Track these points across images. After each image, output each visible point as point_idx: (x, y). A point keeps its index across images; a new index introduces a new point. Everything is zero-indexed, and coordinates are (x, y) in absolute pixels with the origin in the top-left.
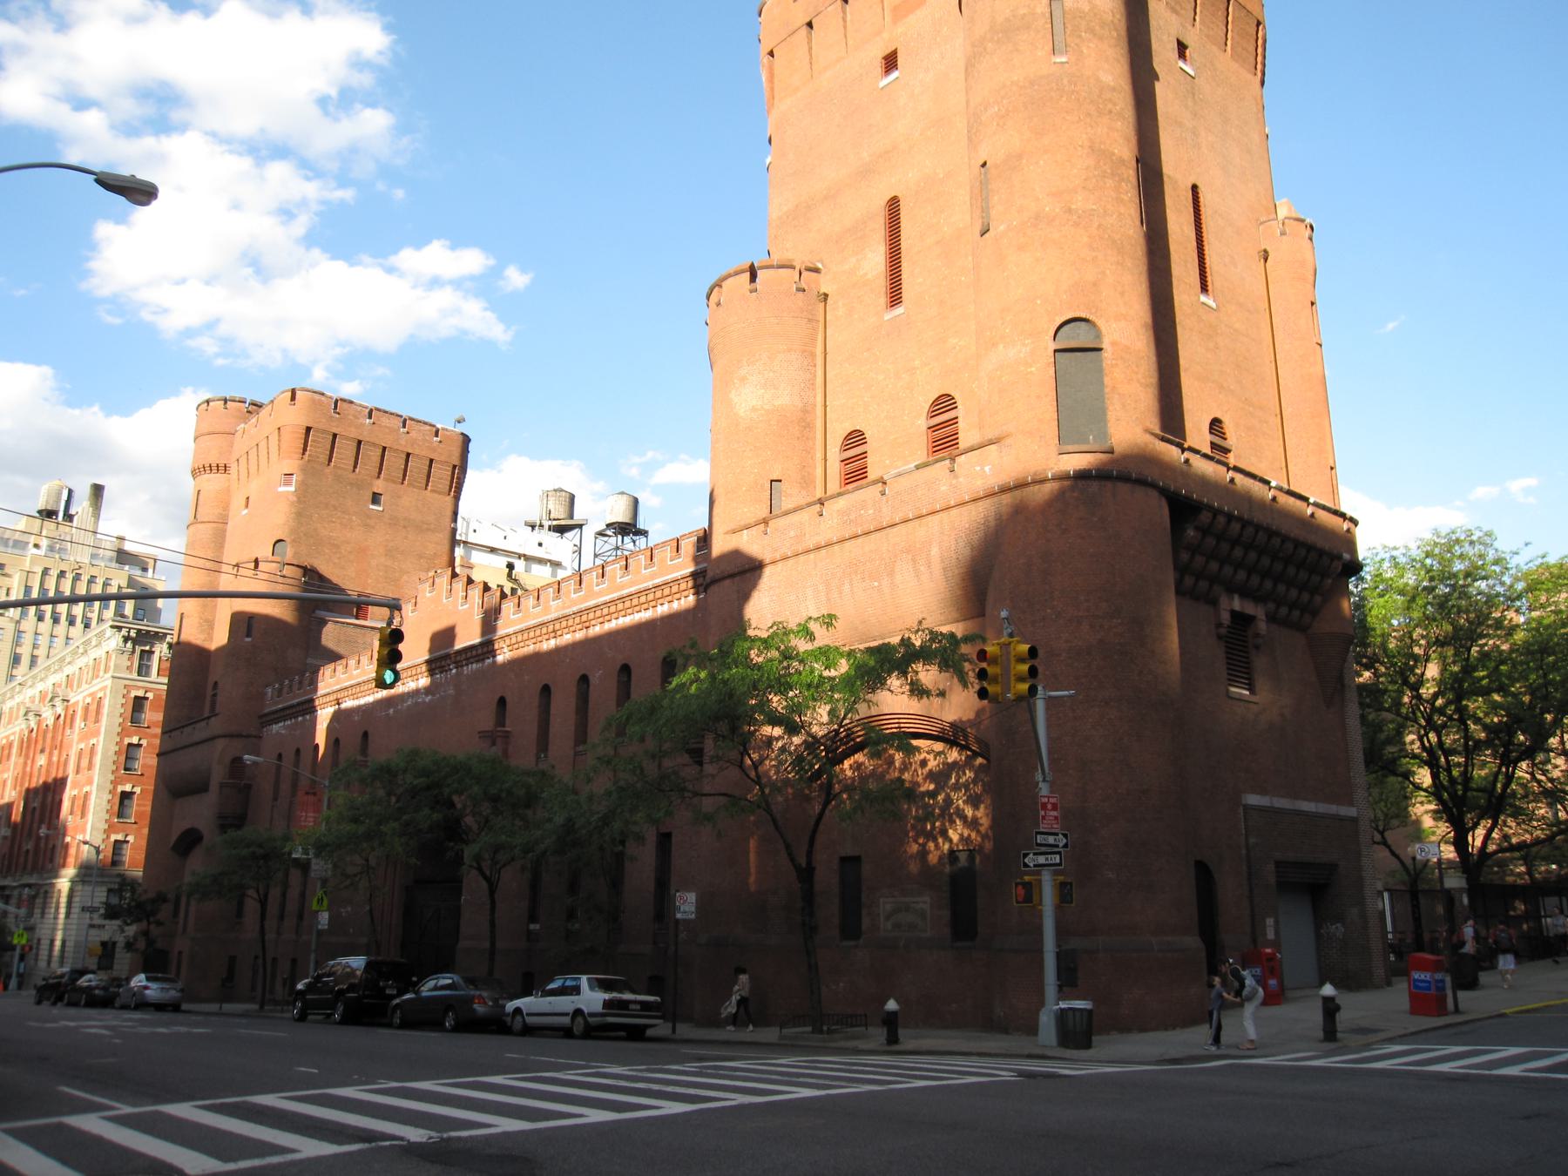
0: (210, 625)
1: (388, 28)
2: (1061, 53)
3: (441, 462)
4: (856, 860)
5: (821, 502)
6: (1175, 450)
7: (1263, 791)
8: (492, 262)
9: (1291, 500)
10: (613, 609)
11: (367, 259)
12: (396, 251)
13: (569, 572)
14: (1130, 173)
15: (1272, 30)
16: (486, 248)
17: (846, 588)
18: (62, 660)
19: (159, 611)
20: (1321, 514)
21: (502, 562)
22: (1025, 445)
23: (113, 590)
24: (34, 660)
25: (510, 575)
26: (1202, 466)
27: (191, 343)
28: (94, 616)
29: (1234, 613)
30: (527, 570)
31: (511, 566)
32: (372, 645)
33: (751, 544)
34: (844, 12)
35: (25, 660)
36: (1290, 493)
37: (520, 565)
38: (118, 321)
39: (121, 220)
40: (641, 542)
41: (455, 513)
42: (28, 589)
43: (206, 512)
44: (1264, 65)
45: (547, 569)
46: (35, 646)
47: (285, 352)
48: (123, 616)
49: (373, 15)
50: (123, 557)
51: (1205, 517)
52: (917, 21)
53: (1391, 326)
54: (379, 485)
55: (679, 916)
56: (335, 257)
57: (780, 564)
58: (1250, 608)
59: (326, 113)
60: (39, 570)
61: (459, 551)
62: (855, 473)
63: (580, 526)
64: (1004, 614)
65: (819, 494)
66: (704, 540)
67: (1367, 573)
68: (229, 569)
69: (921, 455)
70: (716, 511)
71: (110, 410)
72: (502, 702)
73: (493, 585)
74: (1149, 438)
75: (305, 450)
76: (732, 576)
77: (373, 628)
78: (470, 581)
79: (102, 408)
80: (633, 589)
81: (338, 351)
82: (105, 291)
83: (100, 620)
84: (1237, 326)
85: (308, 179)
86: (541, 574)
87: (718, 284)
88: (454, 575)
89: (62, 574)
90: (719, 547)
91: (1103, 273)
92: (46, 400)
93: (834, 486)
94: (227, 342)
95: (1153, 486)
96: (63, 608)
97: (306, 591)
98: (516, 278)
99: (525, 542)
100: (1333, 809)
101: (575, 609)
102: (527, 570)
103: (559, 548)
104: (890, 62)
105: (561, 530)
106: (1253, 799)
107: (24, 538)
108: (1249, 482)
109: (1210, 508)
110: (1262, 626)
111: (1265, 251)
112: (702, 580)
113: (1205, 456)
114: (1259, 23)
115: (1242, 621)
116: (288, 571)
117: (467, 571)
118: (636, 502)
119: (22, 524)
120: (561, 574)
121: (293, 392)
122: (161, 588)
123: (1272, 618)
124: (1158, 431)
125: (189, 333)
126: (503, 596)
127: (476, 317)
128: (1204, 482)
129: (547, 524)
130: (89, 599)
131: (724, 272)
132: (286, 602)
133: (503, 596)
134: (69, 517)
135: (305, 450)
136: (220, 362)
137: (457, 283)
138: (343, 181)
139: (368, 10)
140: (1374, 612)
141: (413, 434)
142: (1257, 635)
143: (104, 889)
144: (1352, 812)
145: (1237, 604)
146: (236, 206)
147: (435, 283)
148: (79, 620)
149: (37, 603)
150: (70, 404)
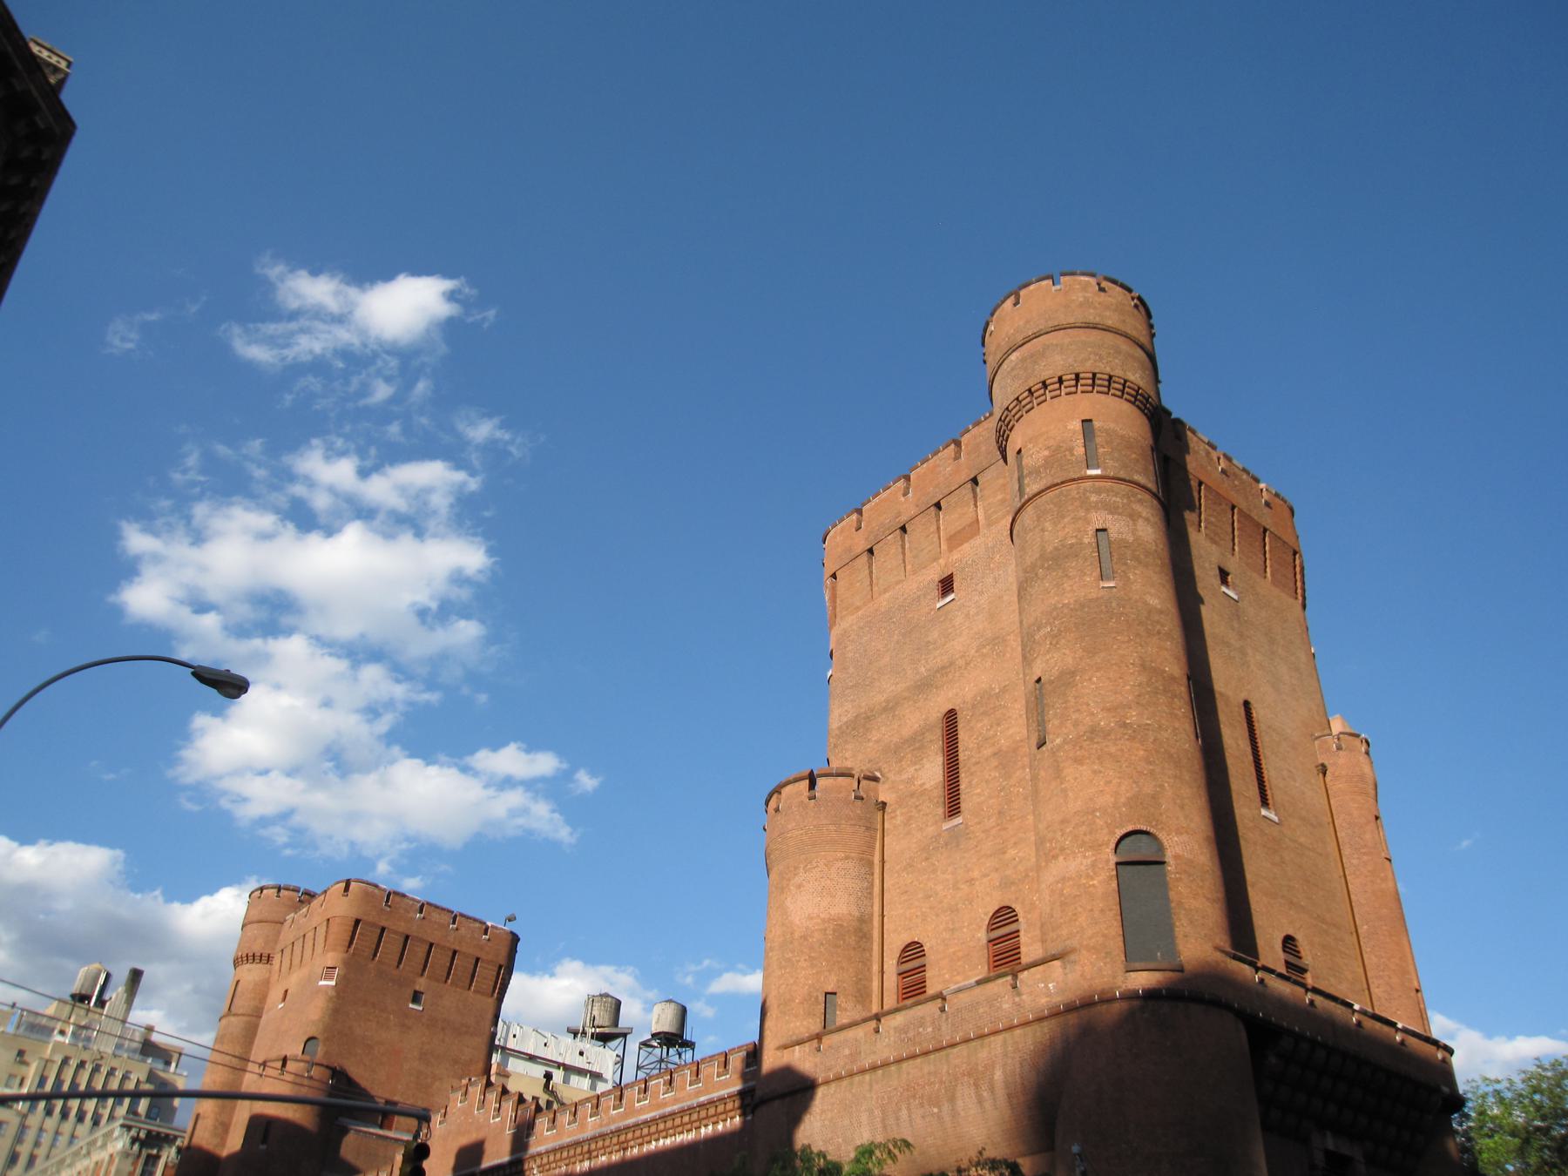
0: (224, 1128)
1: (491, 552)
2: (1109, 579)
3: (489, 962)
5: (877, 1017)
6: (1247, 969)
8: (565, 766)
9: (1378, 1025)
10: (653, 1129)
11: (443, 758)
12: (472, 752)
13: (609, 1086)
14: (1182, 689)
15: (1310, 557)
16: (560, 752)
17: (904, 1113)
18: (62, 1161)
19: (173, 1110)
20: (1412, 1041)
21: (538, 1071)
22: (1086, 959)
23: (130, 1086)
24: (32, 1160)
25: (547, 1086)
26: (1275, 984)
27: (263, 832)
28: (106, 1113)
29: (1329, 1154)
30: (566, 1081)
31: (548, 1076)
32: (392, 1160)
33: (803, 1060)
34: (903, 540)
35: (23, 1161)
36: (1376, 1017)
37: (558, 1075)
38: (196, 808)
39: (218, 712)
40: (688, 1055)
41: (497, 1016)
42: (42, 1081)
43: (242, 1004)
44: (1304, 590)
45: (585, 1083)
46: (37, 1144)
47: (352, 844)
48: (136, 1114)
49: (479, 539)
50: (148, 1048)
52: (969, 550)
53: (1465, 844)
54: (421, 984)
56: (412, 755)
57: (833, 1085)
58: (1346, 1148)
59: (423, 622)
60: (59, 1059)
61: (496, 1058)
62: (913, 988)
63: (625, 1035)
64: (1075, 1149)
65: (875, 1009)
66: (754, 1055)
67: (1471, 1108)
68: (256, 1069)
69: (982, 971)
70: (768, 1024)
71: (170, 898)
73: (528, 1098)
74: (1219, 956)
75: (351, 943)
76: (782, 1096)
77: (397, 1140)
78: (505, 1091)
79: (163, 893)
80: (676, 1107)
81: (404, 846)
82: (190, 779)
83: (111, 1118)
84: (1302, 840)
85: (398, 681)
86: (582, 1084)
87: (777, 791)
88: (489, 1084)
89: (82, 1064)
90: (771, 1060)
91: (1162, 786)
92: (112, 882)
93: (890, 1001)
94: (299, 831)
95: (1228, 1007)
96: (74, 1104)
97: (330, 1095)
98: (586, 781)
99: (566, 1050)
101: (613, 1127)
102: (566, 1081)
103: (603, 1059)
104: (947, 585)
105: (604, 1038)
107: (51, 1024)
108: (1331, 1005)
111: (1323, 765)
112: (749, 1100)
113: (1280, 976)
114: (1295, 553)
116: (315, 1072)
117: (502, 1080)
118: (683, 1011)
119: (51, 1009)
120: (602, 1087)
121: (348, 883)
122: (181, 1084)
124: (1229, 949)
125: (264, 822)
126: (538, 1109)
127: (542, 815)
128: (1282, 1004)
129: (590, 1031)
130: (103, 1096)
131: (784, 780)
132: (308, 1108)
133: (538, 1109)
134: (101, 1003)
135: (351, 943)
136: (288, 852)
137: (530, 785)
138: (431, 685)
139: (475, 535)
140: (1485, 1155)
141: (463, 931)
145: (1330, 1143)
146: (327, 704)
147: (507, 783)
148: (89, 1116)
149: (49, 1097)
150: (136, 888)
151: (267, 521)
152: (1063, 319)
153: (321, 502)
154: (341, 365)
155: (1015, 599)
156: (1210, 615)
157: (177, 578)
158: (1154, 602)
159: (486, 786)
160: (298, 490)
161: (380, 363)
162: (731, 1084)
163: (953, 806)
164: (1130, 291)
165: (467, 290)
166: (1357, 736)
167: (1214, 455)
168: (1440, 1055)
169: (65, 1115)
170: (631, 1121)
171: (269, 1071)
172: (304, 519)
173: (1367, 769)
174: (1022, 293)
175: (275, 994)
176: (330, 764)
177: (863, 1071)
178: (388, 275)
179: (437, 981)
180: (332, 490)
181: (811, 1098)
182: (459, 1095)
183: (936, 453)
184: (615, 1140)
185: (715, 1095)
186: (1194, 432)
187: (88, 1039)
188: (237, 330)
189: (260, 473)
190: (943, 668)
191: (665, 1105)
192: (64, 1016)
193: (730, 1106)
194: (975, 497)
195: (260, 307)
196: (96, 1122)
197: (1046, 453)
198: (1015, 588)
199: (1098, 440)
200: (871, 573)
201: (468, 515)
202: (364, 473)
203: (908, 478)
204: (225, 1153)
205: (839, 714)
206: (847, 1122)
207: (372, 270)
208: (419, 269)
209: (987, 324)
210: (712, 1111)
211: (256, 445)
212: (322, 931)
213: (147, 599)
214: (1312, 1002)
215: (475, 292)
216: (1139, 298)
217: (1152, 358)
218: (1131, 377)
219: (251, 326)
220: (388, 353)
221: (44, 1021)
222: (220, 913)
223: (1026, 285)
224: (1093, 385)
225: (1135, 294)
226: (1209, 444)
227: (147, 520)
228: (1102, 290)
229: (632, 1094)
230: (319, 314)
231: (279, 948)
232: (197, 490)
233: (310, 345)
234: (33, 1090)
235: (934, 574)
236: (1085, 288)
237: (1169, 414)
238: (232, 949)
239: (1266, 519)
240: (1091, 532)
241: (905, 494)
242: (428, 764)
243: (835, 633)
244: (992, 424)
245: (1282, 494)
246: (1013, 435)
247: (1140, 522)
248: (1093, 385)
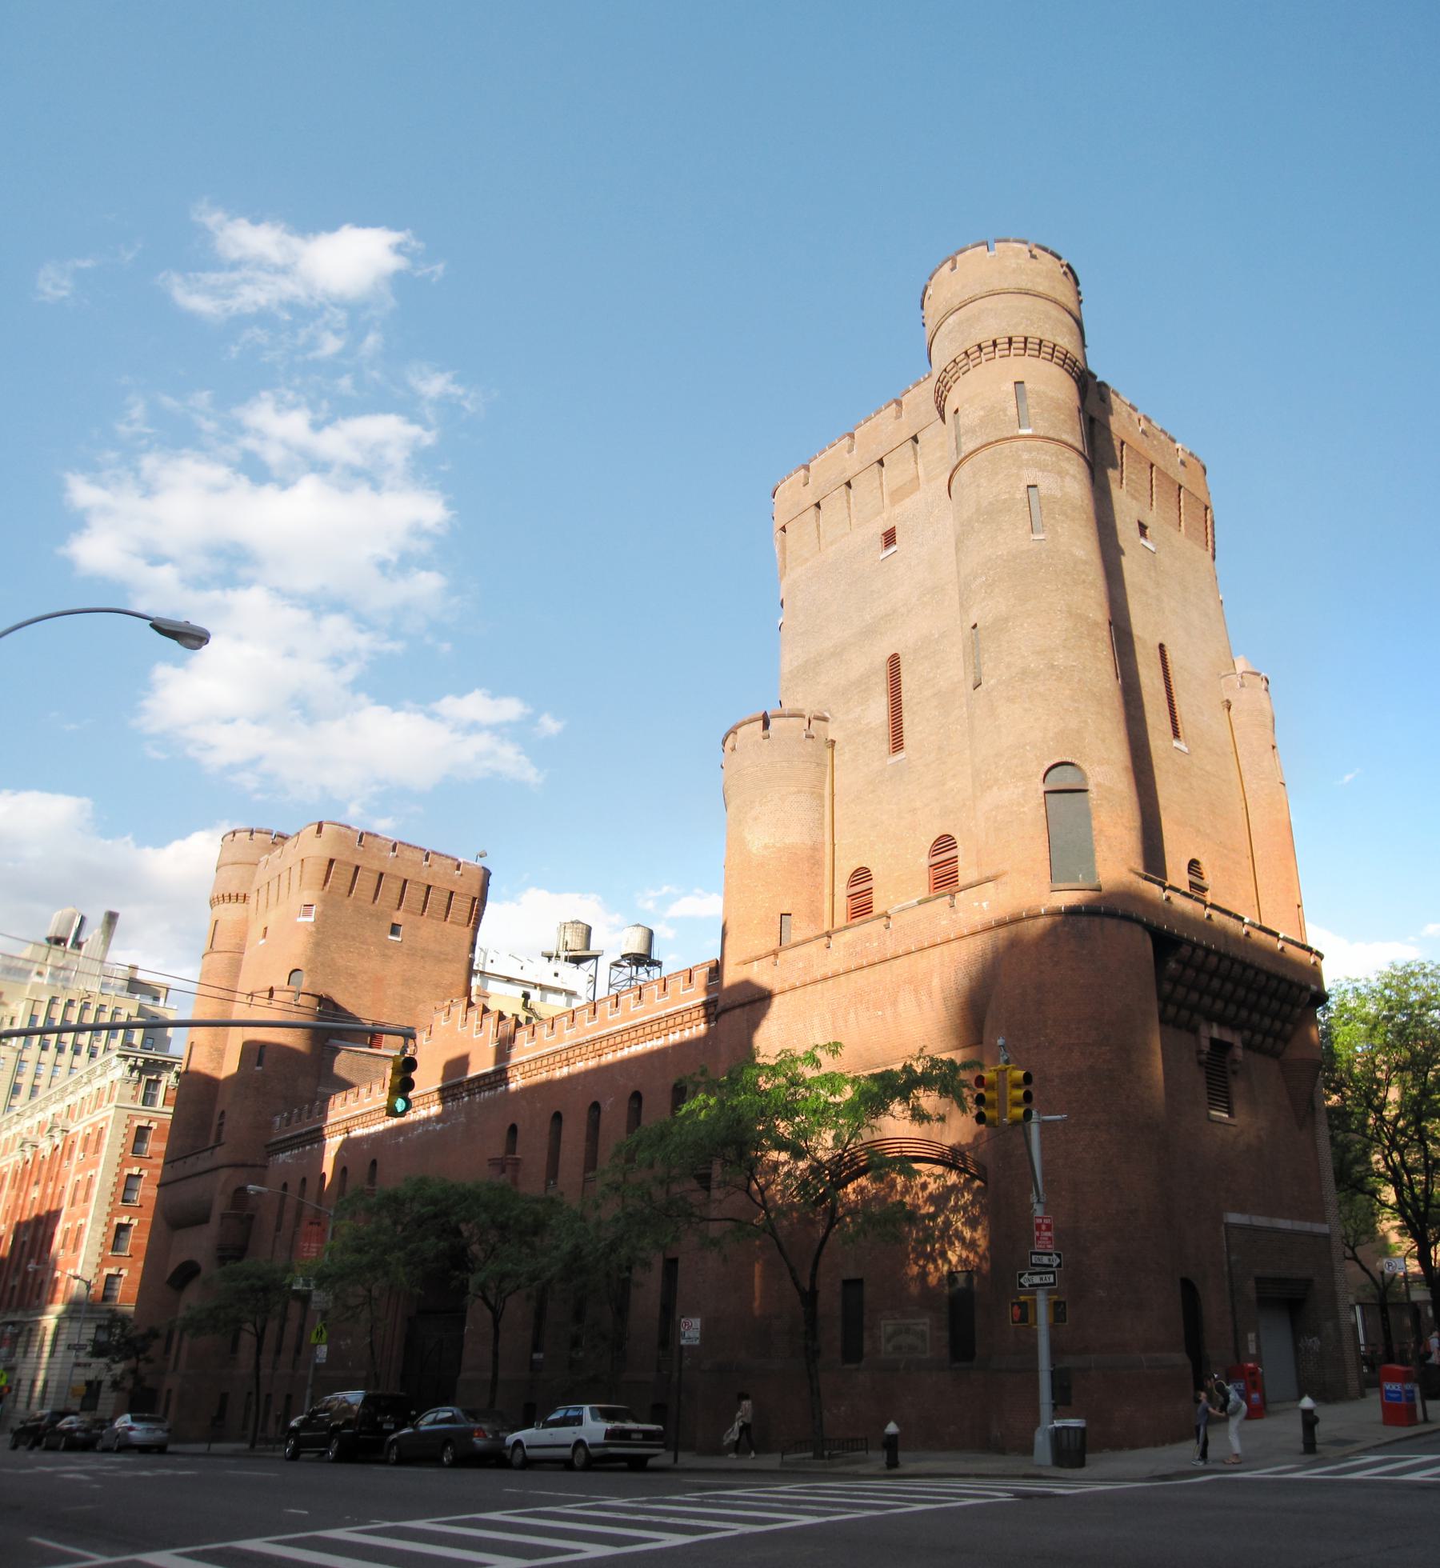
0: (220, 1054)
1: (449, 505)
2: (1039, 532)
4: (859, 1282)
5: (829, 935)
6: (1157, 889)
7: (1242, 1210)
8: (529, 711)
9: (1263, 935)
10: (626, 1037)
13: (583, 1002)
14: (1104, 633)
18: (64, 1089)
19: (168, 1041)
20: (1290, 948)
21: (518, 991)
25: (525, 1004)
28: (101, 1045)
31: (526, 996)
32: (384, 1073)
33: (761, 975)
35: (25, 1090)
37: (535, 995)
39: (179, 663)
40: (655, 972)
41: (474, 944)
43: (224, 942)
46: (37, 1076)
50: (135, 986)
51: (1185, 951)
53: (1347, 778)
54: (398, 917)
55: (683, 1342)
57: (789, 994)
58: (1228, 1036)
60: (46, 999)
61: (476, 981)
62: (861, 908)
63: (596, 957)
64: (1000, 1042)
65: (827, 927)
66: (716, 971)
67: (1333, 1003)
68: (243, 998)
69: (924, 891)
71: (141, 843)
72: (513, 1129)
73: (508, 1014)
74: (1133, 877)
75: (326, 881)
76: (742, 1005)
78: (485, 1010)
80: (646, 1018)
83: (107, 1049)
84: (1208, 768)
85: (361, 631)
88: (470, 1004)
89: (70, 1003)
90: (730, 977)
91: (1085, 722)
93: (841, 920)
95: (1138, 921)
96: (68, 1037)
97: (320, 1020)
98: (550, 725)
99: (543, 972)
100: (1307, 1226)
101: (589, 1037)
103: (575, 978)
104: (890, 538)
105: (577, 960)
106: (1234, 1218)
107: (28, 966)
109: (1189, 942)
110: (1239, 1053)
112: (713, 1010)
113: (1185, 894)
114: (1206, 508)
115: (1220, 1048)
116: (302, 1000)
117: (483, 1001)
118: (651, 934)
119: (27, 952)
120: (576, 1003)
122: (172, 1016)
123: (1248, 1045)
124: (1141, 871)
125: (232, 768)
126: (518, 1024)
127: (510, 759)
128: (1185, 919)
129: (563, 954)
130: (96, 1028)
131: (739, 721)
132: (299, 1031)
133: (518, 1024)
134: (78, 945)
135: (326, 881)
136: (259, 797)
137: (495, 729)
138: (394, 634)
139: (432, 488)
141: (435, 867)
142: (1235, 1061)
143: (93, 1325)
144: (1324, 1229)
145: (1215, 1032)
146: (291, 654)
147: (474, 728)
149: (42, 1032)
151: (219, 474)
152: (997, 285)
153: (273, 455)
154: (287, 317)
155: (953, 551)
156: (1130, 566)
157: (135, 526)
158: (1080, 553)
159: (454, 731)
160: (250, 443)
161: (327, 316)
162: (697, 996)
163: (897, 743)
164: (1059, 258)
165: (414, 243)
166: (1258, 674)
167: (1135, 416)
168: (1312, 959)
169: (60, 1049)
170: (605, 1032)
171: (256, 1000)
172: (256, 471)
173: (1266, 704)
174: (959, 258)
175: (256, 931)
176: (297, 712)
177: (816, 982)
178: (332, 225)
179: (414, 913)
180: (285, 443)
181: (769, 1006)
182: (443, 1014)
183: (878, 413)
184: (591, 1048)
185: (681, 1007)
186: (1117, 395)
187: (67, 979)
188: (176, 279)
189: (210, 426)
190: (888, 615)
191: (634, 1017)
192: (41, 958)
193: (695, 1015)
194: (915, 454)
195: (199, 257)
196: (93, 1055)
197: (982, 413)
198: (953, 540)
199: (1029, 401)
200: (818, 526)
201: (424, 468)
202: (316, 426)
203: (852, 436)
204: (222, 1075)
205: (790, 659)
206: (801, 1026)
207: (315, 217)
208: (364, 221)
209: (926, 288)
210: (679, 1020)
211: (203, 398)
212: (296, 870)
213: (99, 552)
214: (1209, 917)
215: (421, 245)
216: (1068, 266)
217: (1079, 323)
218: (1060, 341)
219: (191, 275)
220: (336, 305)
221: (20, 964)
222: (193, 857)
223: (962, 252)
224: (1025, 349)
225: (1064, 262)
226: (1131, 406)
227: (92, 470)
228: (1033, 257)
229: (605, 1008)
230: (261, 264)
231: (254, 888)
232: (145, 442)
233: (254, 296)
234: (25, 1026)
235: (879, 527)
236: (1017, 255)
237: (1095, 377)
238: (207, 893)
239: (1182, 479)
240: (1023, 488)
241: (850, 451)
242: (395, 711)
243: (784, 585)
244: (931, 384)
245: (1196, 454)
246: (950, 396)
247: (1068, 479)
248: (1025, 349)
